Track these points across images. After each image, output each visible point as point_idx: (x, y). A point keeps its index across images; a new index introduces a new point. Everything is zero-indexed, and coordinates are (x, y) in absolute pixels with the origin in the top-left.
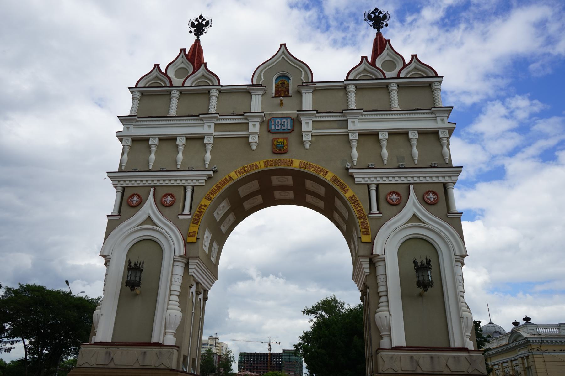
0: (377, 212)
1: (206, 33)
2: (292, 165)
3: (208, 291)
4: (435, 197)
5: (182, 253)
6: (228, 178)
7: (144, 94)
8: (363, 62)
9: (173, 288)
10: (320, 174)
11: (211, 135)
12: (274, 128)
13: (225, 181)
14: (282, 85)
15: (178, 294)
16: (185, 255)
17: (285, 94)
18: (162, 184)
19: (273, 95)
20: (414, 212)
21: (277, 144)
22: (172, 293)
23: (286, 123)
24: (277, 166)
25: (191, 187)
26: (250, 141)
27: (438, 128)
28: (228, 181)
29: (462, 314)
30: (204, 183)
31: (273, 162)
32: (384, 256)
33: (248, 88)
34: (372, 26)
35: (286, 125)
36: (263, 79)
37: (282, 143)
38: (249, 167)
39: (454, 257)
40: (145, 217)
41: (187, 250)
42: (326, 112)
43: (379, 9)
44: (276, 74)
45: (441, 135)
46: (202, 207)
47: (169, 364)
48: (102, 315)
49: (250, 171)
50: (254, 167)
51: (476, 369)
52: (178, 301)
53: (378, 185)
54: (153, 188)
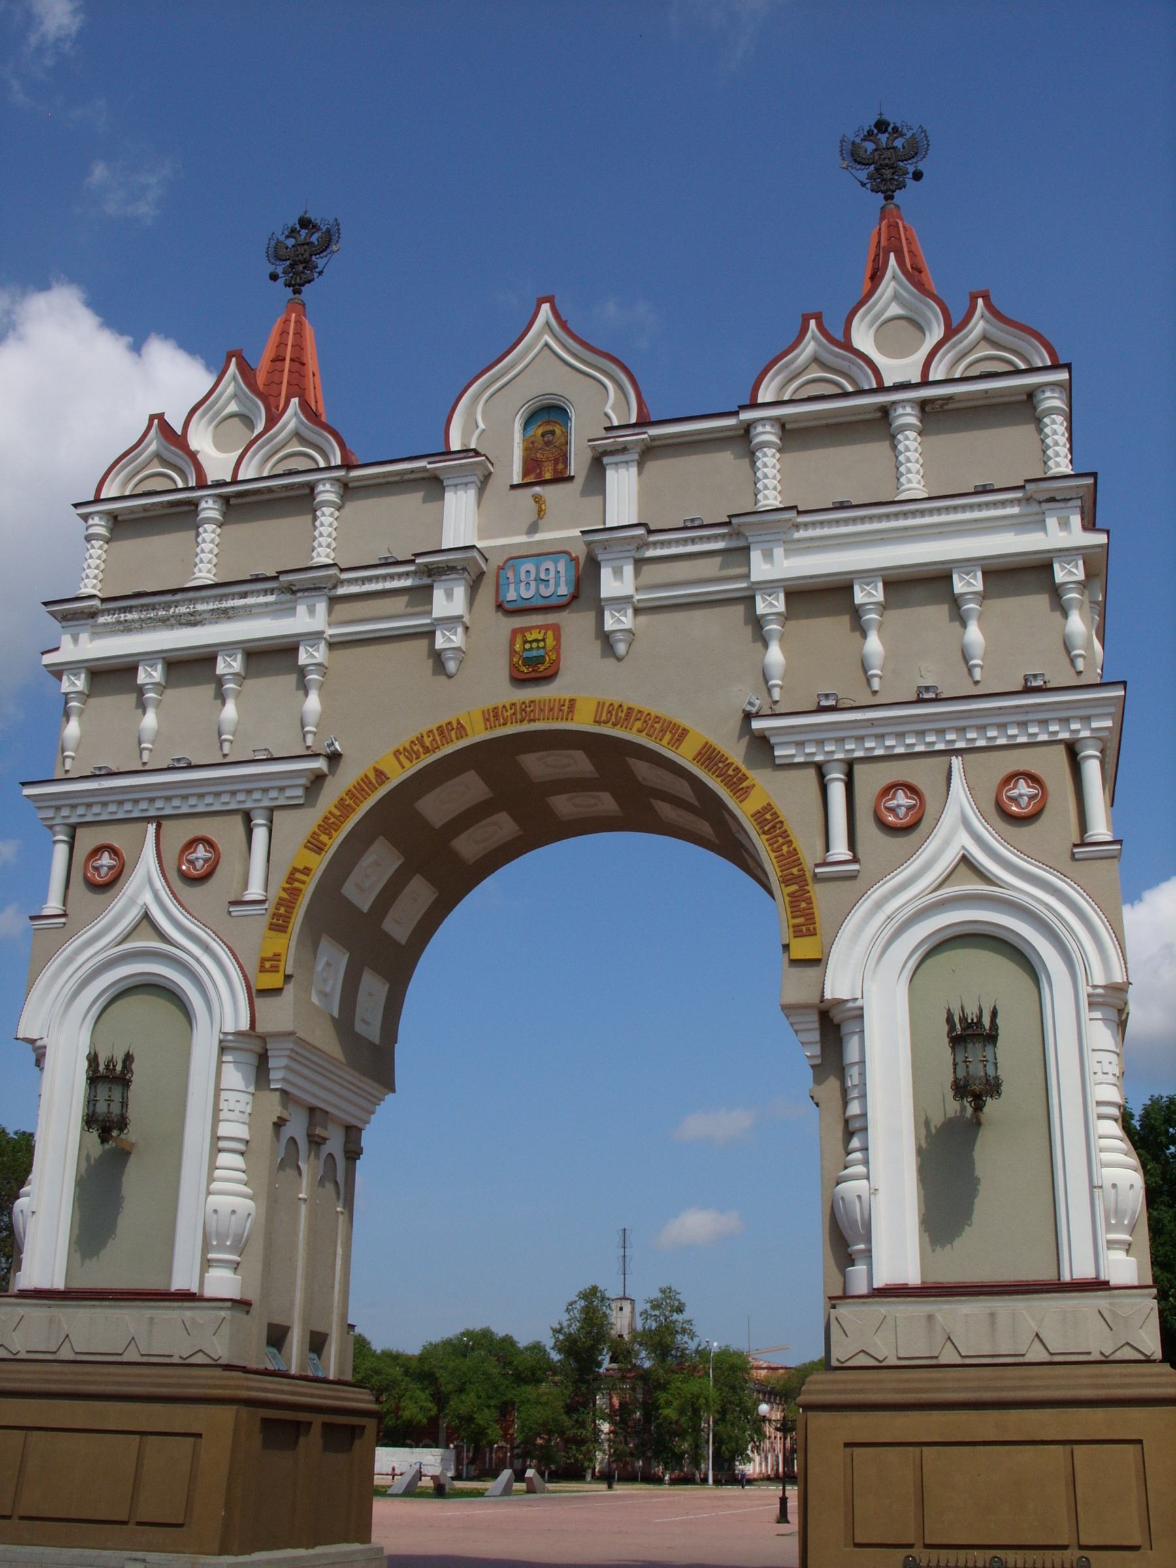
0: (848, 856)
1: (320, 273)
2: (572, 716)
3: (360, 1130)
4: (1033, 791)
5: (244, 1025)
6: (372, 776)
7: (350, 485)
8: (809, 334)
9: (224, 1129)
10: (660, 740)
11: (320, 636)
12: (515, 594)
13: (363, 787)
14: (546, 439)
15: (241, 1147)
16: (250, 1028)
17: (555, 470)
18: (179, 807)
19: (517, 479)
20: (963, 848)
21: (525, 650)
22: (222, 1144)
23: (552, 573)
24: (526, 721)
25: (266, 813)
26: (606, 629)
27: (1049, 551)
28: (374, 785)
29: (1099, 1176)
30: (301, 797)
31: (513, 711)
32: (858, 1003)
33: (429, 466)
34: (868, 186)
35: (552, 582)
36: (482, 426)
37: (541, 644)
38: (436, 733)
39: (1084, 990)
40: (133, 914)
41: (257, 1015)
42: (973, 490)
43: (891, 122)
44: (522, 407)
45: (1062, 574)
46: (298, 876)
47: (220, 1352)
48: (33, 1213)
49: (441, 747)
50: (453, 733)
51: (1128, 1343)
52: (243, 1166)
53: (850, 767)
54: (154, 825)
